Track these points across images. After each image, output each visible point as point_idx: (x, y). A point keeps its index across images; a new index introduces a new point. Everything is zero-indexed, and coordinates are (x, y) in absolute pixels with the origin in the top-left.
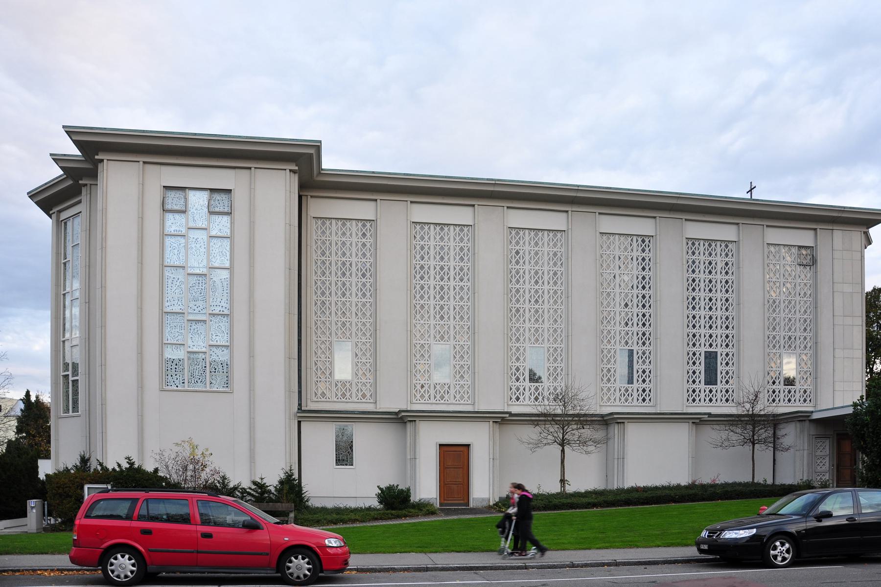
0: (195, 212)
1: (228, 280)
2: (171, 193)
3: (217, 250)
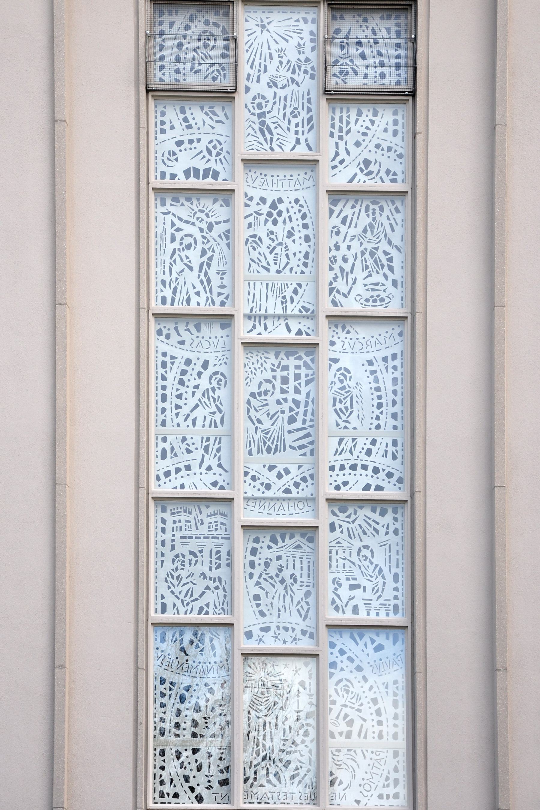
0: (269, 94)
1: (397, 363)
2: (173, 18)
3: (355, 244)
